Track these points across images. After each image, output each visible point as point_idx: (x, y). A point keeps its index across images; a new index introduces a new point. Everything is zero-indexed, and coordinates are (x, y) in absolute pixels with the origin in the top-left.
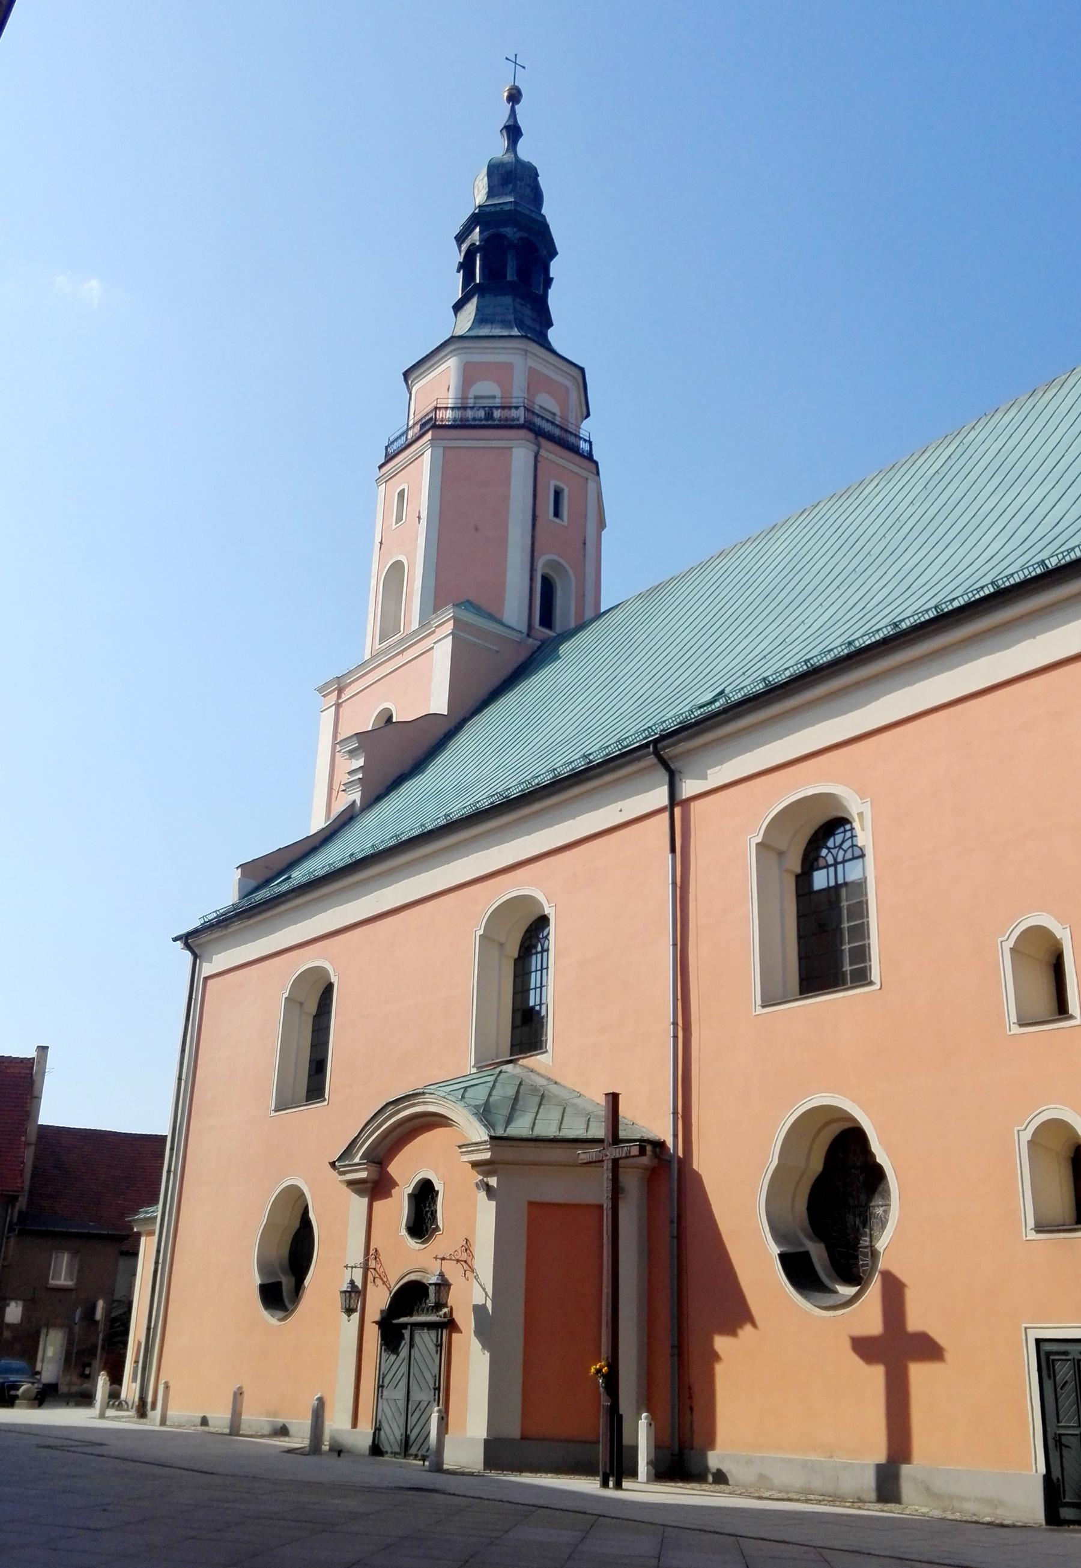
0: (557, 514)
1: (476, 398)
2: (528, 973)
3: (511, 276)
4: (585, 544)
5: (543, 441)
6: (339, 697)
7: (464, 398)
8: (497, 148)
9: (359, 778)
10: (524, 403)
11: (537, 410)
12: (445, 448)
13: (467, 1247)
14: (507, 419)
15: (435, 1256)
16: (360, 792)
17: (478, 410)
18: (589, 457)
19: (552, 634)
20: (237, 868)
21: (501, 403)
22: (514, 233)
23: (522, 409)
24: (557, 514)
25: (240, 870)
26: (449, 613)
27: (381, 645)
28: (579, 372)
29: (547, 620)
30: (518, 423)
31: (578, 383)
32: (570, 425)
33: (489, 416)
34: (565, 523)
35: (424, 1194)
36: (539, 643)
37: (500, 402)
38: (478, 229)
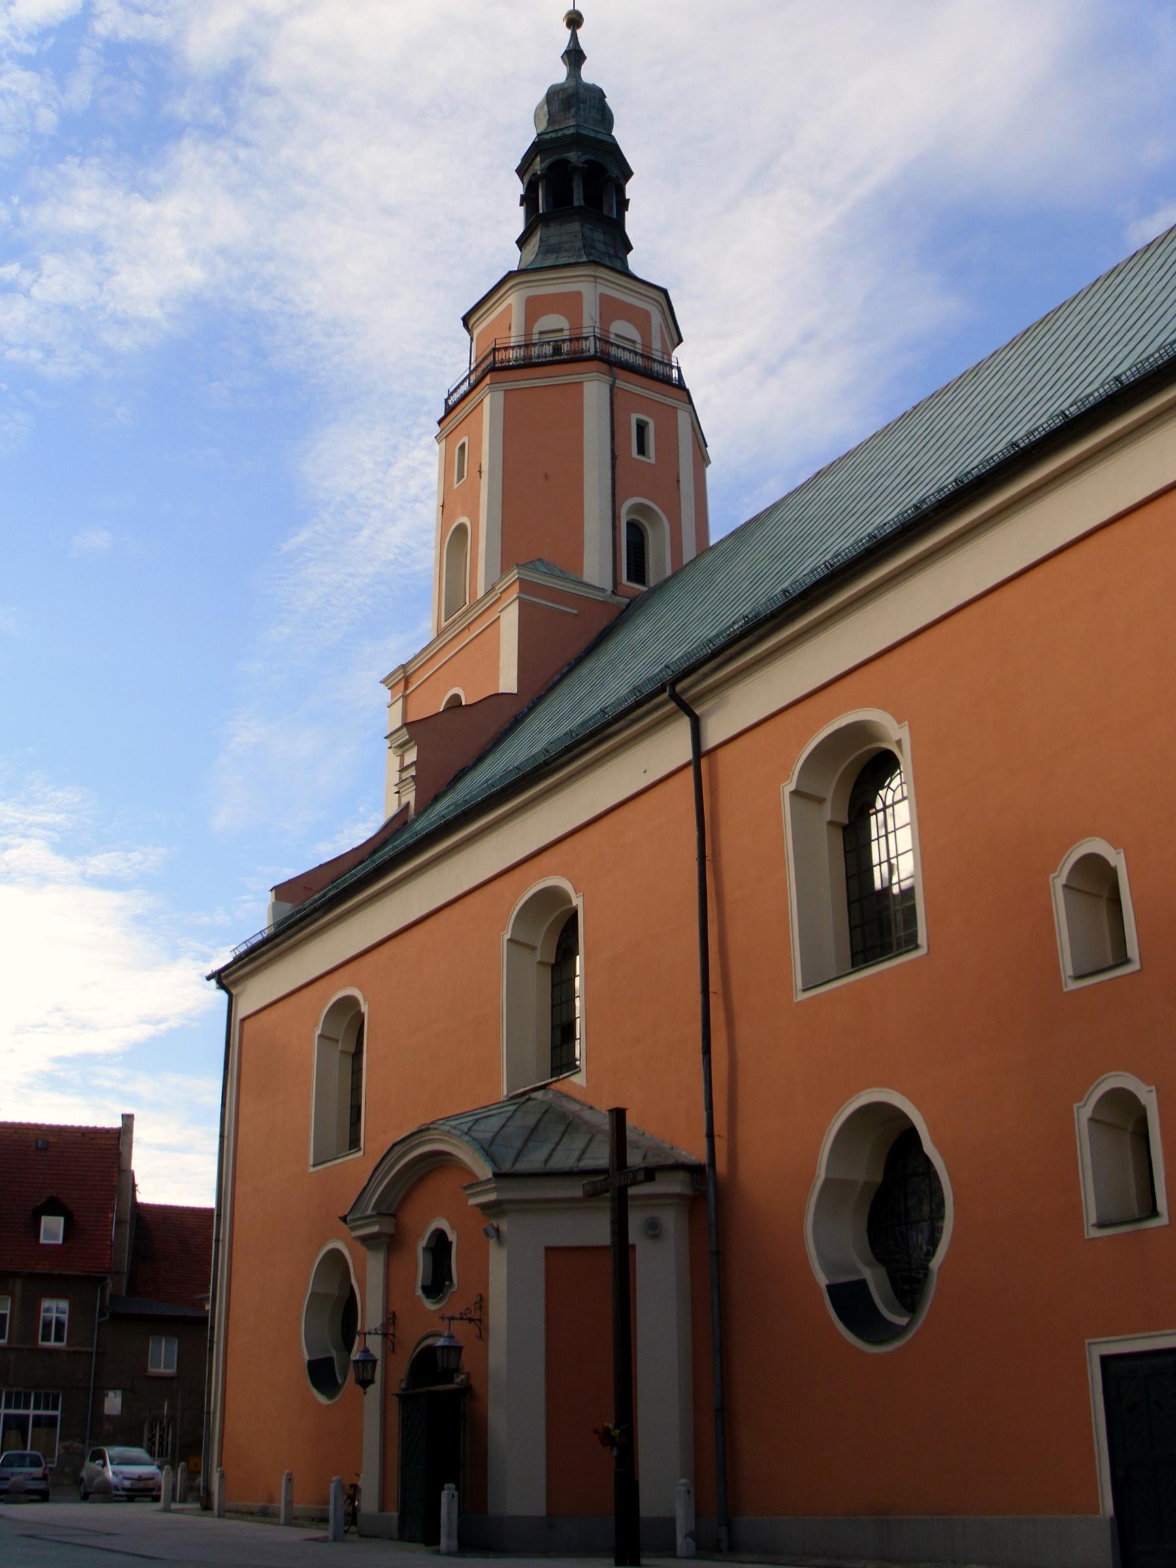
0: (642, 450)
1: (541, 333)
2: (572, 979)
3: (578, 200)
4: (678, 481)
5: (615, 370)
6: (406, 688)
7: (528, 333)
8: (559, 74)
9: (412, 776)
10: (594, 332)
11: (613, 339)
12: (505, 391)
13: (482, 1302)
14: (575, 352)
15: (441, 1315)
16: (414, 792)
17: (542, 346)
18: (681, 386)
19: (644, 589)
20: (271, 890)
21: (570, 335)
22: (579, 157)
23: (592, 339)
24: (642, 450)
25: (274, 891)
26: (514, 575)
27: (448, 622)
28: (663, 296)
29: (638, 571)
30: (588, 354)
31: (661, 305)
32: (654, 352)
33: (557, 350)
34: (652, 460)
35: (440, 1246)
36: (628, 601)
37: (537, 338)
38: (538, 159)
